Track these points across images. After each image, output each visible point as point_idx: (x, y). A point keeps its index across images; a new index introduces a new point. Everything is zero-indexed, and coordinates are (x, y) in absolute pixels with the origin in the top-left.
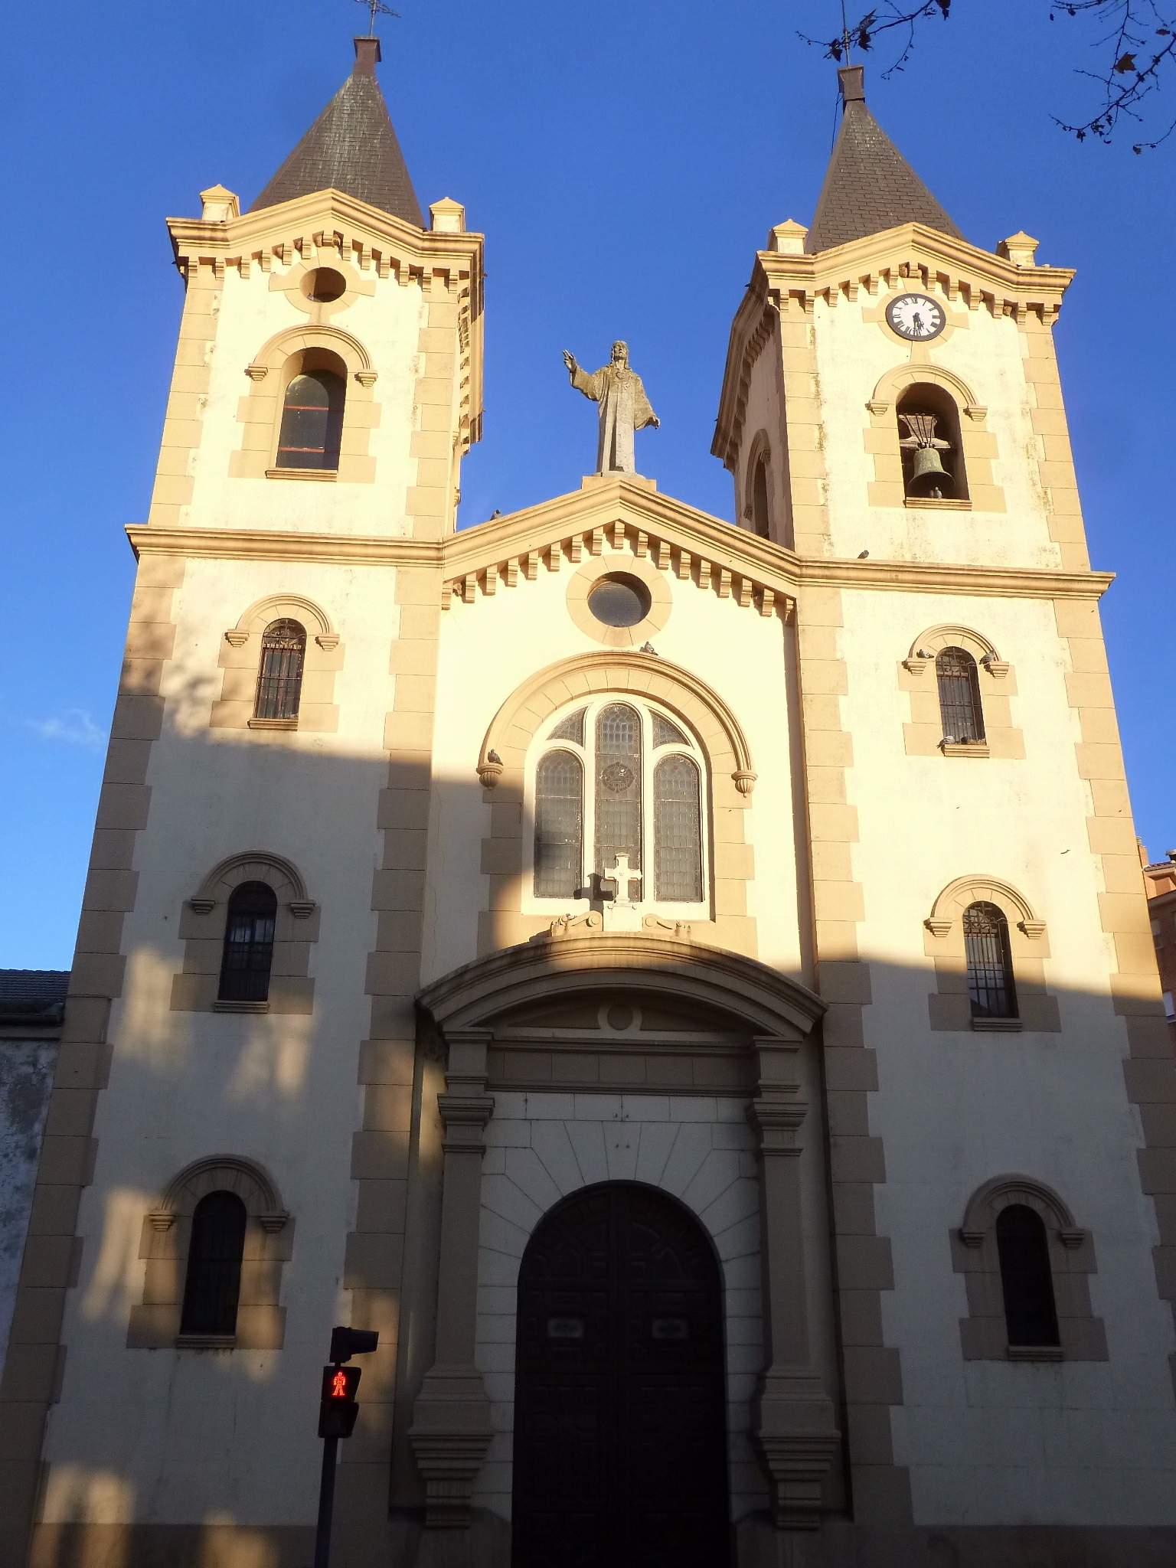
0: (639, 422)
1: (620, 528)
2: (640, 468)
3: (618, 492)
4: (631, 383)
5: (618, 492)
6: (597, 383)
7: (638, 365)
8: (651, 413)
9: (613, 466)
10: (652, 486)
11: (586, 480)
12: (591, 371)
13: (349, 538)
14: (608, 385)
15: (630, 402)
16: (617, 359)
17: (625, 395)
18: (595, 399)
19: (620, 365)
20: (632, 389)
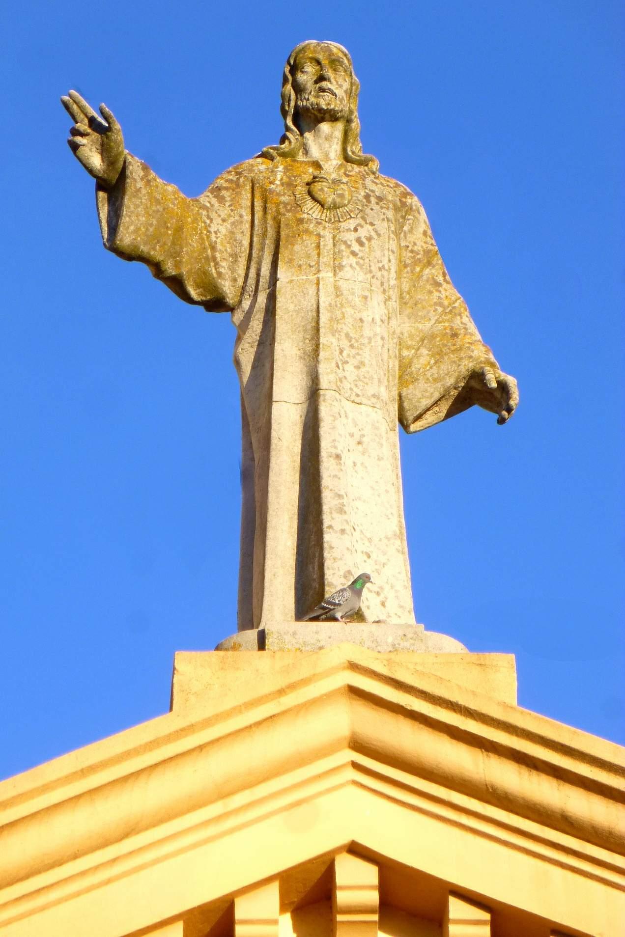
0: (423, 394)
1: (356, 884)
2: (434, 606)
3: (344, 718)
4: (381, 220)
5: (344, 718)
6: (219, 231)
7: (395, 142)
8: (478, 353)
9: (312, 602)
10: (493, 683)
11: (192, 669)
12: (194, 181)
13: (103, 104)
14: (274, 238)
15: (376, 309)
16: (307, 118)
17: (353, 277)
18: (216, 304)
19: (325, 145)
20: (384, 252)
